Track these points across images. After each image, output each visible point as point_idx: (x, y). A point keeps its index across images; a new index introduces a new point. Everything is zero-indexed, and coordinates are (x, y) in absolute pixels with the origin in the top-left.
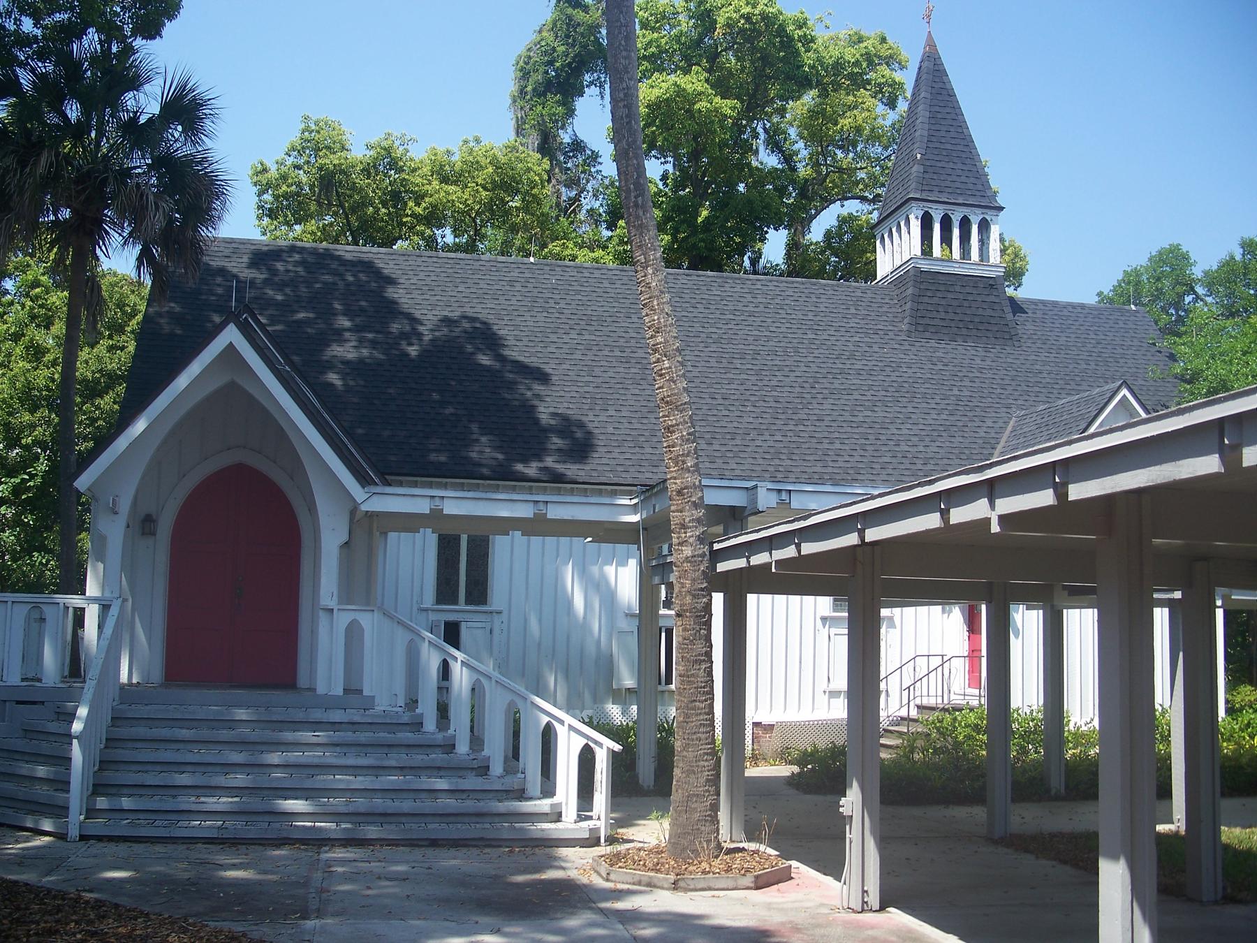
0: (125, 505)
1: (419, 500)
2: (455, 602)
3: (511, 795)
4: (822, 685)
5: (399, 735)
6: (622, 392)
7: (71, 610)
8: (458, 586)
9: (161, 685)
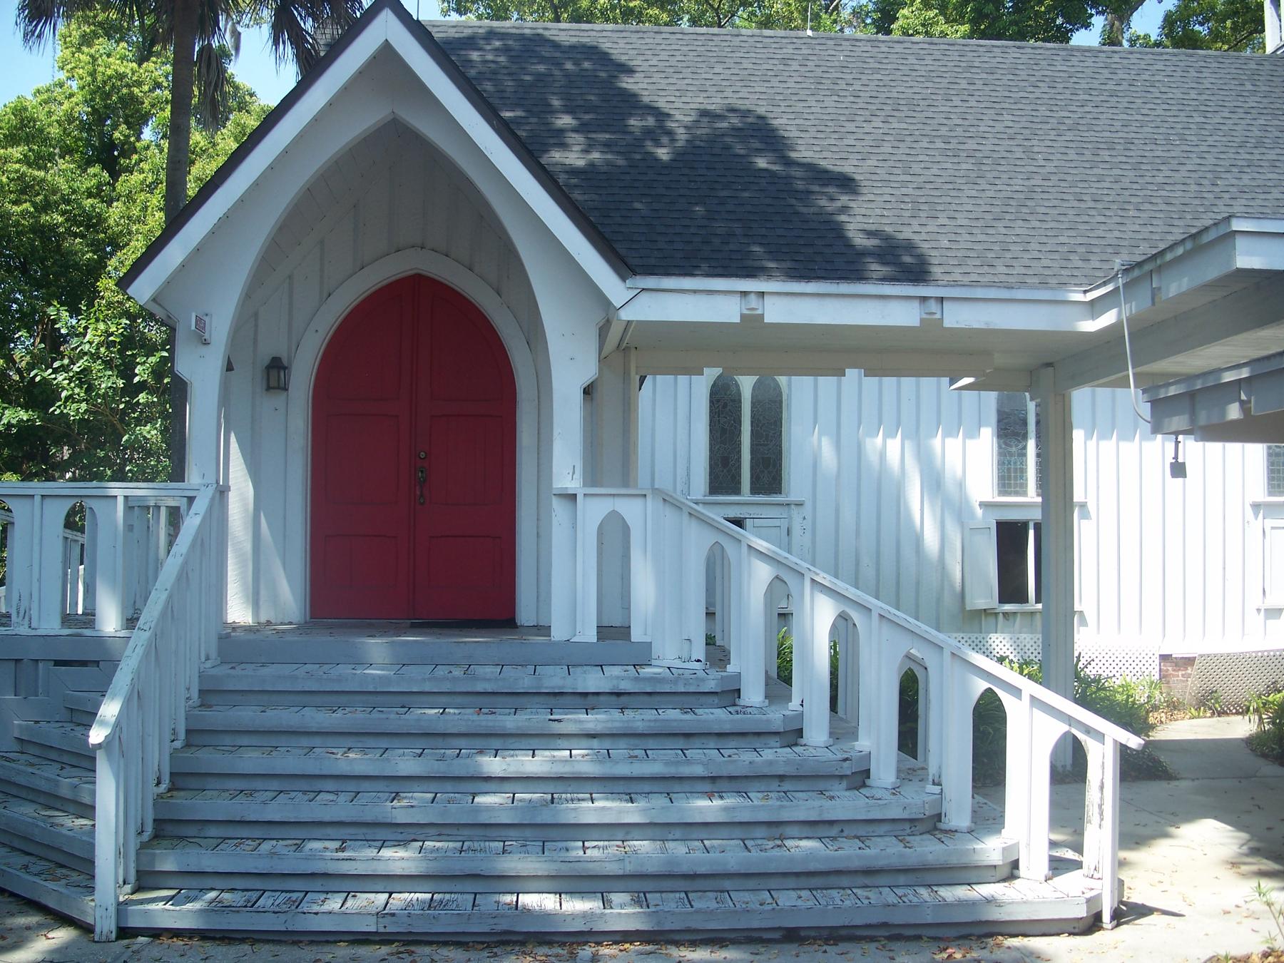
0: (220, 329)
1: (719, 299)
2: (736, 490)
3: (920, 827)
4: (1255, 600)
5: (768, 754)
6: (953, 193)
7: (163, 511)
8: (739, 467)
9: (303, 628)
